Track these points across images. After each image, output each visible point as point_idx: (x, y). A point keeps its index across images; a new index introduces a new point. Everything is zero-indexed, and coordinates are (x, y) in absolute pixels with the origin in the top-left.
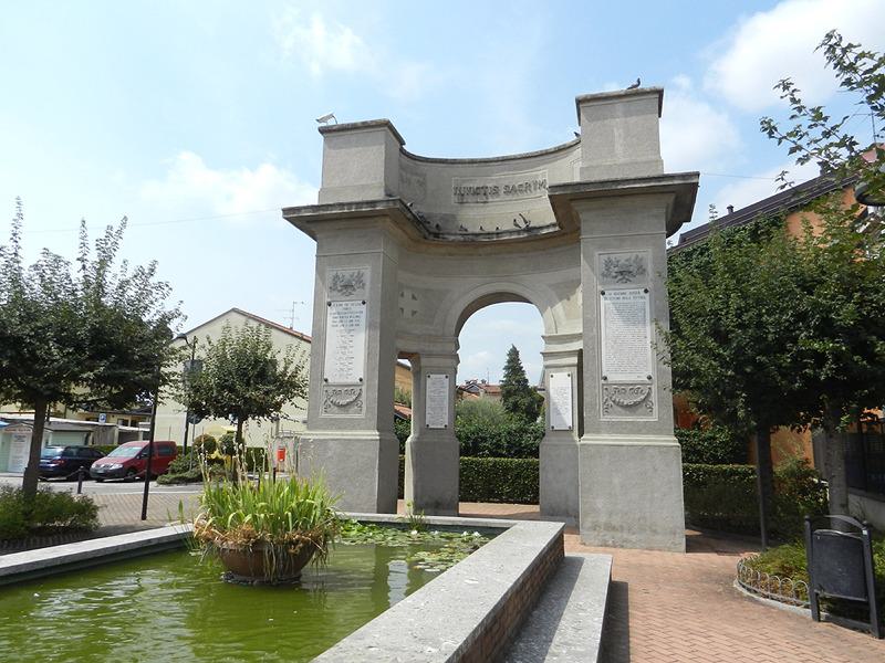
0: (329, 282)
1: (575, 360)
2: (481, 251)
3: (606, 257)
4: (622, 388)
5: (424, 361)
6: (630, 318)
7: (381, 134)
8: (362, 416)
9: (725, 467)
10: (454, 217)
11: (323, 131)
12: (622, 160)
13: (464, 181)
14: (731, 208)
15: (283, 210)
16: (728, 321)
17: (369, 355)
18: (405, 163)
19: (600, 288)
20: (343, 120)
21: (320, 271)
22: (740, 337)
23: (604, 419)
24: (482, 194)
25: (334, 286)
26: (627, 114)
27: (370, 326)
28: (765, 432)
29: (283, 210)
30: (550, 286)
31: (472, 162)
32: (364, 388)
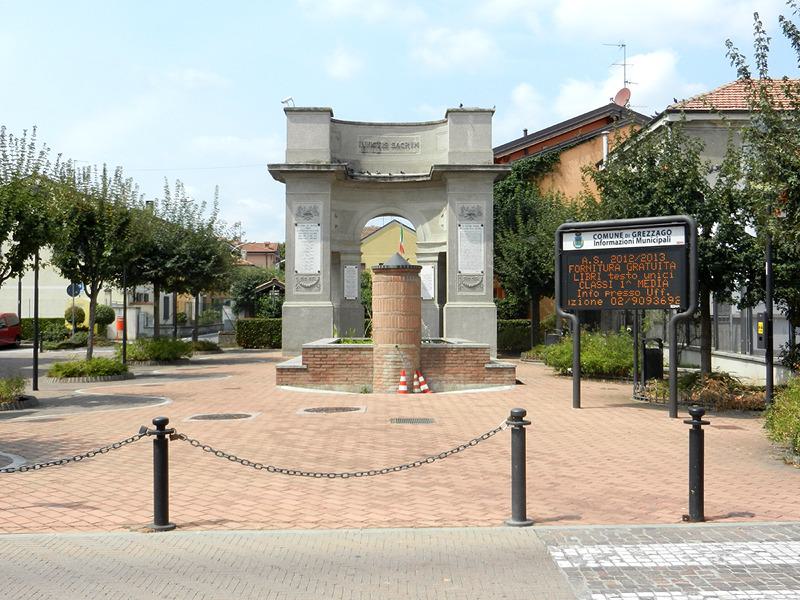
0: (295, 211)
1: (436, 258)
2: (379, 186)
3: (461, 206)
4: (468, 277)
5: (342, 257)
6: (473, 239)
7: (326, 117)
8: (320, 292)
9: (514, 321)
10: (358, 161)
11: (286, 110)
12: (471, 149)
13: (366, 138)
14: (526, 131)
15: (269, 166)
16: (523, 256)
17: (324, 257)
18: (339, 129)
19: (458, 222)
20: (299, 105)
21: (289, 204)
22: (527, 263)
23: (459, 294)
24: (377, 147)
25: (300, 214)
26: (476, 122)
27: (324, 239)
28: (537, 300)
29: (269, 166)
30: (422, 211)
31: (371, 124)
32: (321, 277)
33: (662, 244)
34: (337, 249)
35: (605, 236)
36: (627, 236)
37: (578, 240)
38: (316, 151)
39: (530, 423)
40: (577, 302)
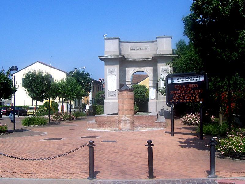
8: (116, 97)
33: (197, 81)
34: (122, 83)
35: (180, 79)
36: (187, 78)
37: (172, 81)
38: (114, 51)
39: (154, 145)
40: (182, 101)
